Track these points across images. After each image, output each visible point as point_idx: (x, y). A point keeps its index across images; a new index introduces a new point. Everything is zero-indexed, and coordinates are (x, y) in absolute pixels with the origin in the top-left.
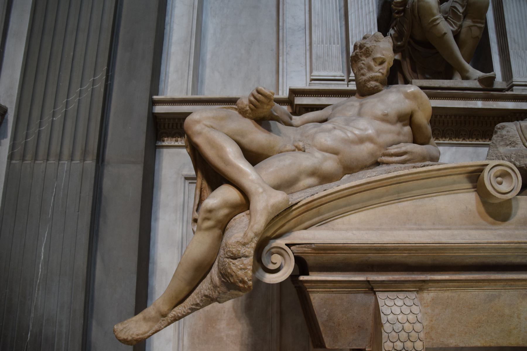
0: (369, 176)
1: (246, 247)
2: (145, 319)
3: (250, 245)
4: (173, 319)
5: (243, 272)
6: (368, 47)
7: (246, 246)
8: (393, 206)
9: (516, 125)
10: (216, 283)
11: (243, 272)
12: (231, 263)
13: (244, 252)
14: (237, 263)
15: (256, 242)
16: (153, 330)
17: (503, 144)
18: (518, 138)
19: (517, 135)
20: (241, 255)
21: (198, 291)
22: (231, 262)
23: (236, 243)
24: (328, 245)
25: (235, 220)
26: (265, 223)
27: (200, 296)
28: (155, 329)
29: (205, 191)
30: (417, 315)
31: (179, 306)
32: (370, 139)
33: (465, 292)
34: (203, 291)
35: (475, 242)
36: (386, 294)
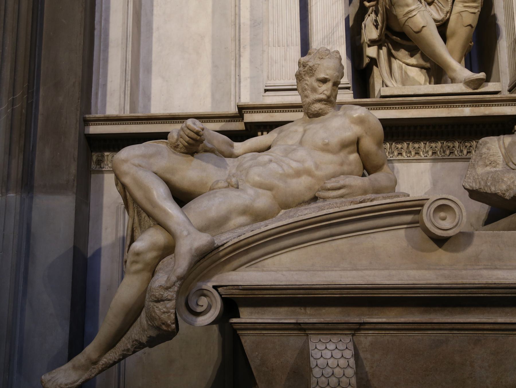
0: (300, 214)
1: (168, 291)
2: (75, 368)
3: (173, 289)
4: (104, 366)
5: (166, 315)
6: (311, 66)
7: (169, 290)
8: (327, 244)
9: (499, 140)
10: (144, 327)
11: (166, 316)
12: (155, 307)
13: (166, 296)
14: (160, 307)
15: (178, 285)
16: (83, 379)
17: (482, 164)
18: (500, 156)
19: (498, 153)
20: (164, 299)
21: (129, 336)
22: (155, 306)
23: (159, 287)
24: (255, 286)
25: (163, 262)
26: (188, 267)
27: (131, 341)
28: (84, 378)
29: (136, 231)
30: (349, 360)
31: (109, 352)
32: (308, 173)
33: (407, 337)
34: (133, 336)
35: (412, 283)
36: (320, 337)
